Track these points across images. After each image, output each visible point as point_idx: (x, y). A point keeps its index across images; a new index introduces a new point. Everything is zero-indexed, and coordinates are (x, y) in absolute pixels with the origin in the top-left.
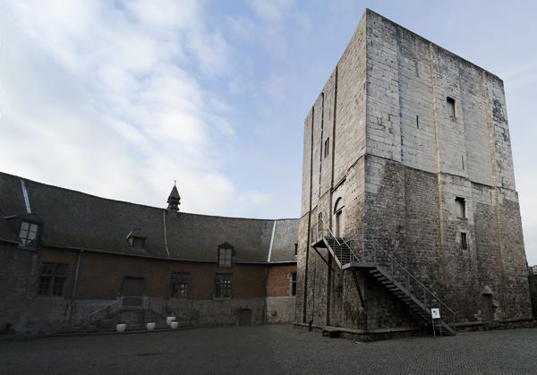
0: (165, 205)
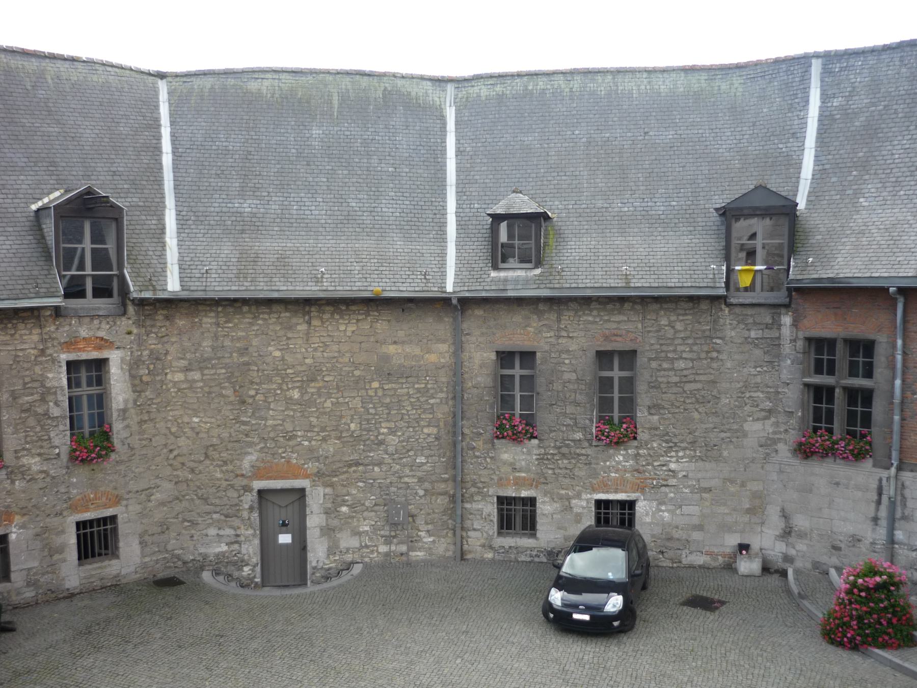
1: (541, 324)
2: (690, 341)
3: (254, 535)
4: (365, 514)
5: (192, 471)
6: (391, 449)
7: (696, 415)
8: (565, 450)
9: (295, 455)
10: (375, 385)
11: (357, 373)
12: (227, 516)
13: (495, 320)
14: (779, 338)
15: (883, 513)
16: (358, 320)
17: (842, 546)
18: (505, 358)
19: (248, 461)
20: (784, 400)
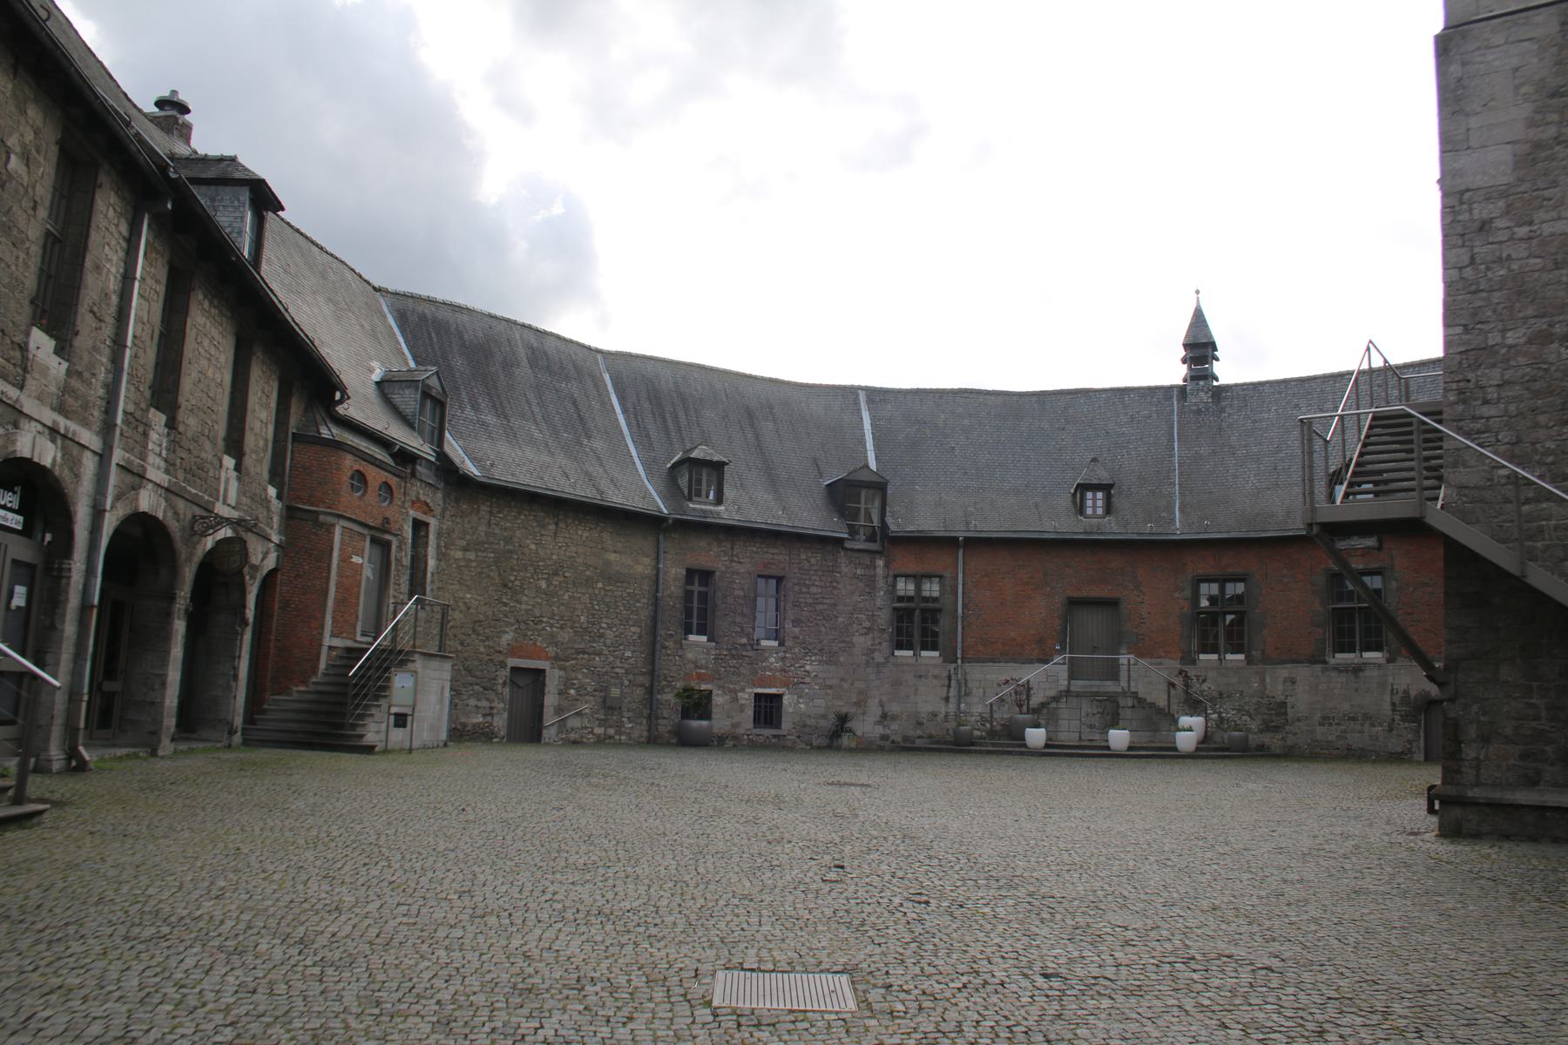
0: (1173, 373)
2: (820, 573)
3: (504, 710)
4: (587, 698)
5: (462, 644)
6: (608, 642)
7: (823, 629)
8: (734, 652)
9: (540, 639)
10: (600, 585)
11: (588, 573)
12: (485, 689)
14: (875, 576)
15: (953, 692)
16: (591, 529)
18: (691, 573)
19: (507, 638)
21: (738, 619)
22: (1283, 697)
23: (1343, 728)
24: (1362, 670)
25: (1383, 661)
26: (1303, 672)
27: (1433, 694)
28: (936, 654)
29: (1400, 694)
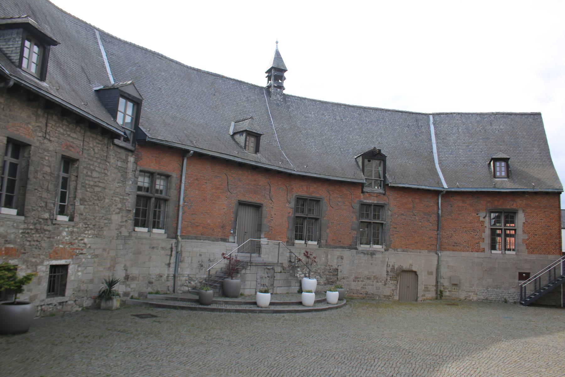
0: (263, 82)
1: (37, 124)
2: (99, 161)
7: (97, 208)
8: (38, 226)
13: (10, 110)
15: (173, 260)
17: (154, 281)
20: (126, 203)
21: (45, 195)
22: (337, 266)
23: (364, 283)
24: (374, 254)
25: (383, 250)
26: (347, 253)
27: (404, 268)
28: (162, 231)
29: (391, 267)
